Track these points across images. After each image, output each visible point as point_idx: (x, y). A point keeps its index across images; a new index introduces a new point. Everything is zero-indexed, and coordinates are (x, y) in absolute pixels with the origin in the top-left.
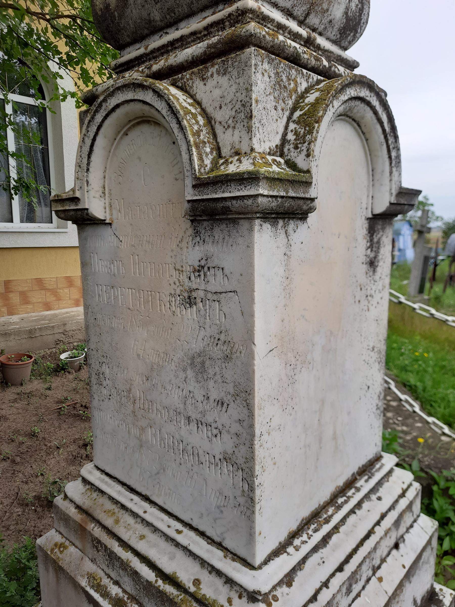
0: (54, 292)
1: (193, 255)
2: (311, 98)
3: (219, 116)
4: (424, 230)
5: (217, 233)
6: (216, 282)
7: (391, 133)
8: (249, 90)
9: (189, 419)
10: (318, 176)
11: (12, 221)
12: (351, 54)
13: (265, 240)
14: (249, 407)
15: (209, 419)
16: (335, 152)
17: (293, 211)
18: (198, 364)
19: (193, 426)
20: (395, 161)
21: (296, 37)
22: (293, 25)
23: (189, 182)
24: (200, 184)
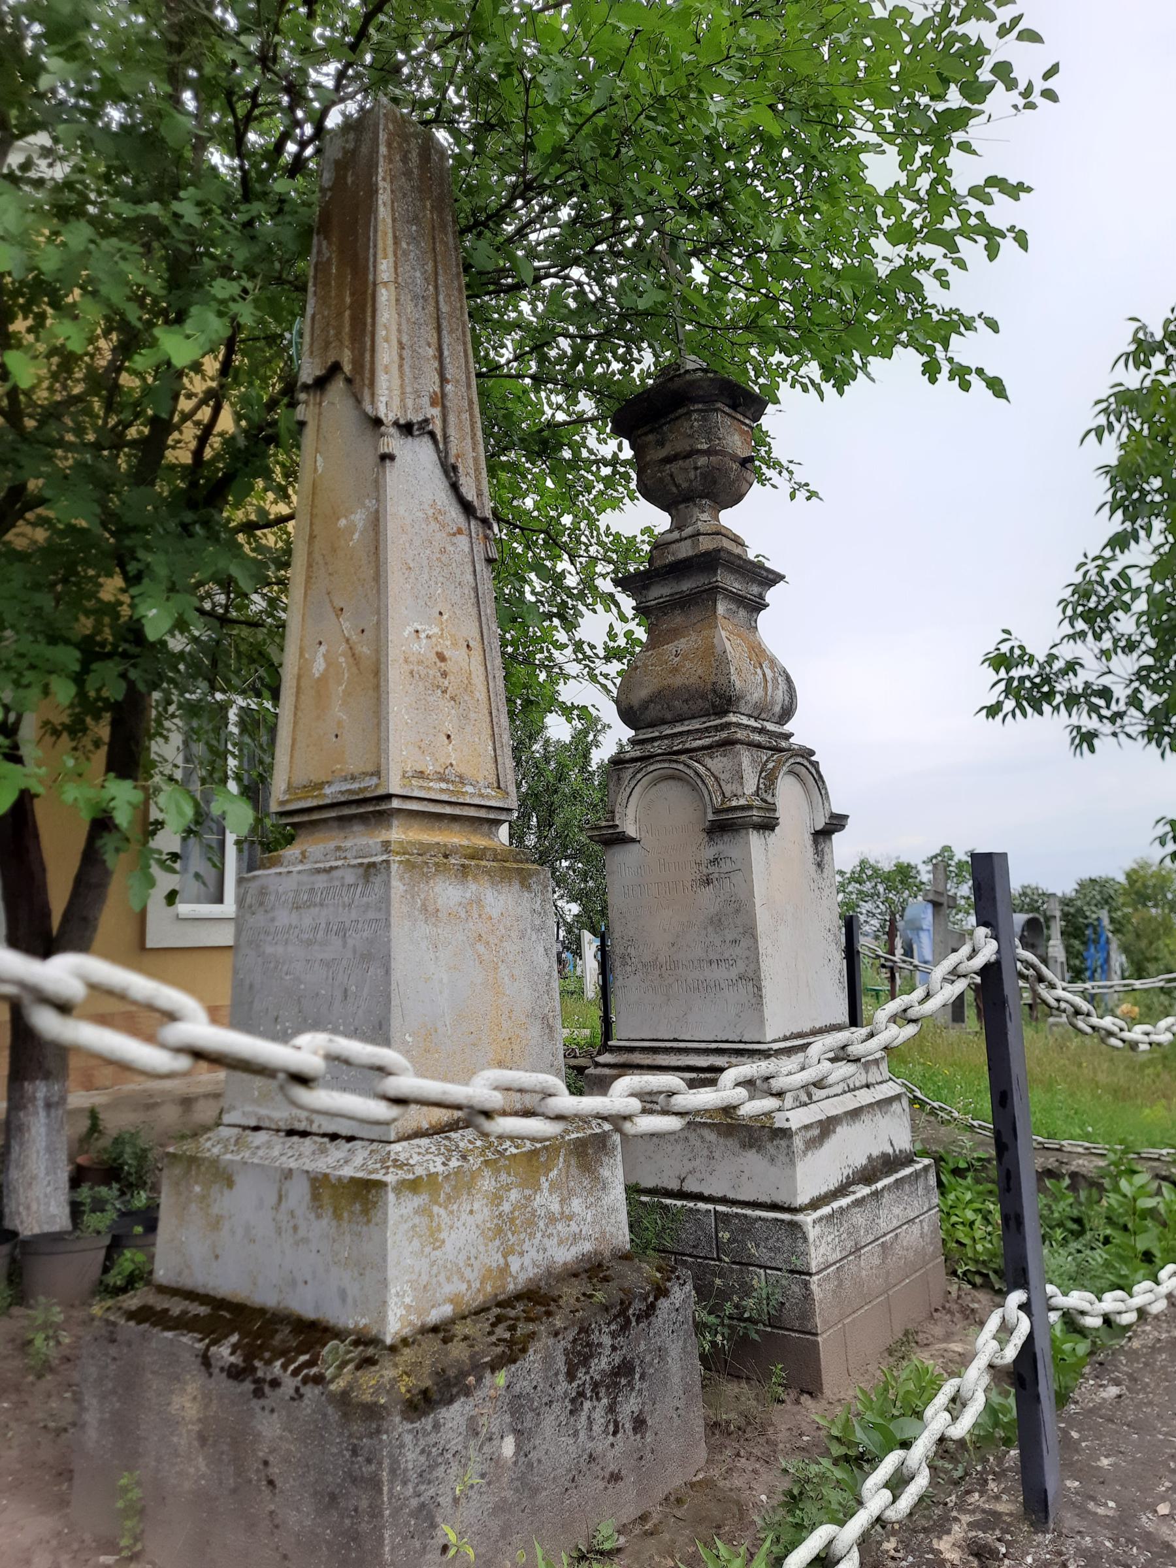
1: (710, 852)
2: (770, 765)
3: (722, 776)
4: (944, 900)
5: (726, 838)
6: (726, 867)
7: (819, 779)
8: (740, 765)
9: (711, 962)
10: (779, 806)
11: (220, 900)
12: (788, 728)
13: (755, 839)
14: (754, 937)
15: (726, 956)
16: (788, 795)
17: (768, 825)
18: (716, 922)
19: (714, 965)
21: (754, 730)
22: (752, 723)
23: (710, 811)
24: (717, 812)
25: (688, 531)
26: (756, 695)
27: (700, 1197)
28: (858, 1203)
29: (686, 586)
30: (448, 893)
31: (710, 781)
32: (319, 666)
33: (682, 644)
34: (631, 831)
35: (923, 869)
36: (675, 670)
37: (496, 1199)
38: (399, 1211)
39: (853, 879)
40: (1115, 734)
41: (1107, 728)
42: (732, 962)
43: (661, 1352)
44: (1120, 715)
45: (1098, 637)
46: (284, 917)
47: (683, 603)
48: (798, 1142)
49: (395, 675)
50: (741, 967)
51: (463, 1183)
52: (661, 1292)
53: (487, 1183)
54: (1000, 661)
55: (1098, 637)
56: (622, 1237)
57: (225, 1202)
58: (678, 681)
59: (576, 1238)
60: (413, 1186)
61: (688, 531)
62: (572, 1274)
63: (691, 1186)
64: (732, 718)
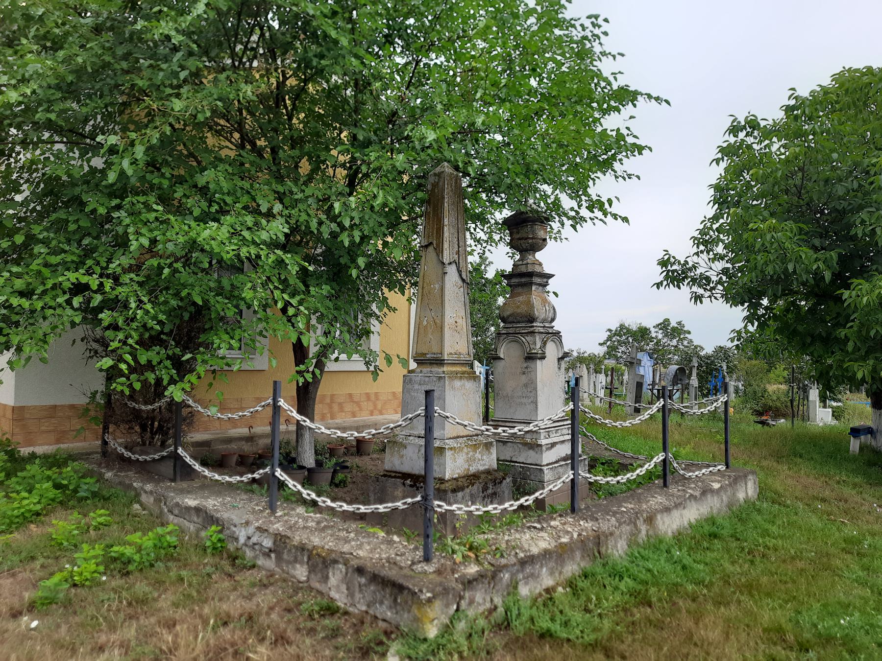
0: (358, 404)
1: (525, 365)
4: (635, 361)
13: (538, 362)
20: (563, 347)
25: (525, 262)
26: (542, 316)
27: (516, 462)
28: (561, 466)
29: (523, 280)
30: (457, 383)
31: (526, 344)
32: (425, 323)
33: (521, 298)
34: (502, 356)
35: (653, 330)
36: (518, 307)
37: (467, 454)
38: (448, 454)
39: (615, 334)
40: (710, 297)
41: (708, 294)
42: (529, 397)
43: (503, 492)
44: (713, 288)
45: (708, 253)
46: (416, 387)
47: (522, 285)
48: (544, 448)
49: (446, 329)
50: (532, 399)
51: (461, 449)
52: (504, 479)
53: (465, 450)
54: (663, 263)
55: (708, 253)
56: (495, 466)
57: (404, 452)
58: (519, 311)
59: (484, 465)
60: (451, 449)
61: (525, 262)
62: (484, 472)
63: (514, 459)
64: (535, 324)
